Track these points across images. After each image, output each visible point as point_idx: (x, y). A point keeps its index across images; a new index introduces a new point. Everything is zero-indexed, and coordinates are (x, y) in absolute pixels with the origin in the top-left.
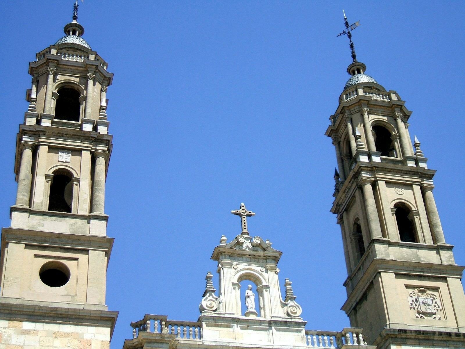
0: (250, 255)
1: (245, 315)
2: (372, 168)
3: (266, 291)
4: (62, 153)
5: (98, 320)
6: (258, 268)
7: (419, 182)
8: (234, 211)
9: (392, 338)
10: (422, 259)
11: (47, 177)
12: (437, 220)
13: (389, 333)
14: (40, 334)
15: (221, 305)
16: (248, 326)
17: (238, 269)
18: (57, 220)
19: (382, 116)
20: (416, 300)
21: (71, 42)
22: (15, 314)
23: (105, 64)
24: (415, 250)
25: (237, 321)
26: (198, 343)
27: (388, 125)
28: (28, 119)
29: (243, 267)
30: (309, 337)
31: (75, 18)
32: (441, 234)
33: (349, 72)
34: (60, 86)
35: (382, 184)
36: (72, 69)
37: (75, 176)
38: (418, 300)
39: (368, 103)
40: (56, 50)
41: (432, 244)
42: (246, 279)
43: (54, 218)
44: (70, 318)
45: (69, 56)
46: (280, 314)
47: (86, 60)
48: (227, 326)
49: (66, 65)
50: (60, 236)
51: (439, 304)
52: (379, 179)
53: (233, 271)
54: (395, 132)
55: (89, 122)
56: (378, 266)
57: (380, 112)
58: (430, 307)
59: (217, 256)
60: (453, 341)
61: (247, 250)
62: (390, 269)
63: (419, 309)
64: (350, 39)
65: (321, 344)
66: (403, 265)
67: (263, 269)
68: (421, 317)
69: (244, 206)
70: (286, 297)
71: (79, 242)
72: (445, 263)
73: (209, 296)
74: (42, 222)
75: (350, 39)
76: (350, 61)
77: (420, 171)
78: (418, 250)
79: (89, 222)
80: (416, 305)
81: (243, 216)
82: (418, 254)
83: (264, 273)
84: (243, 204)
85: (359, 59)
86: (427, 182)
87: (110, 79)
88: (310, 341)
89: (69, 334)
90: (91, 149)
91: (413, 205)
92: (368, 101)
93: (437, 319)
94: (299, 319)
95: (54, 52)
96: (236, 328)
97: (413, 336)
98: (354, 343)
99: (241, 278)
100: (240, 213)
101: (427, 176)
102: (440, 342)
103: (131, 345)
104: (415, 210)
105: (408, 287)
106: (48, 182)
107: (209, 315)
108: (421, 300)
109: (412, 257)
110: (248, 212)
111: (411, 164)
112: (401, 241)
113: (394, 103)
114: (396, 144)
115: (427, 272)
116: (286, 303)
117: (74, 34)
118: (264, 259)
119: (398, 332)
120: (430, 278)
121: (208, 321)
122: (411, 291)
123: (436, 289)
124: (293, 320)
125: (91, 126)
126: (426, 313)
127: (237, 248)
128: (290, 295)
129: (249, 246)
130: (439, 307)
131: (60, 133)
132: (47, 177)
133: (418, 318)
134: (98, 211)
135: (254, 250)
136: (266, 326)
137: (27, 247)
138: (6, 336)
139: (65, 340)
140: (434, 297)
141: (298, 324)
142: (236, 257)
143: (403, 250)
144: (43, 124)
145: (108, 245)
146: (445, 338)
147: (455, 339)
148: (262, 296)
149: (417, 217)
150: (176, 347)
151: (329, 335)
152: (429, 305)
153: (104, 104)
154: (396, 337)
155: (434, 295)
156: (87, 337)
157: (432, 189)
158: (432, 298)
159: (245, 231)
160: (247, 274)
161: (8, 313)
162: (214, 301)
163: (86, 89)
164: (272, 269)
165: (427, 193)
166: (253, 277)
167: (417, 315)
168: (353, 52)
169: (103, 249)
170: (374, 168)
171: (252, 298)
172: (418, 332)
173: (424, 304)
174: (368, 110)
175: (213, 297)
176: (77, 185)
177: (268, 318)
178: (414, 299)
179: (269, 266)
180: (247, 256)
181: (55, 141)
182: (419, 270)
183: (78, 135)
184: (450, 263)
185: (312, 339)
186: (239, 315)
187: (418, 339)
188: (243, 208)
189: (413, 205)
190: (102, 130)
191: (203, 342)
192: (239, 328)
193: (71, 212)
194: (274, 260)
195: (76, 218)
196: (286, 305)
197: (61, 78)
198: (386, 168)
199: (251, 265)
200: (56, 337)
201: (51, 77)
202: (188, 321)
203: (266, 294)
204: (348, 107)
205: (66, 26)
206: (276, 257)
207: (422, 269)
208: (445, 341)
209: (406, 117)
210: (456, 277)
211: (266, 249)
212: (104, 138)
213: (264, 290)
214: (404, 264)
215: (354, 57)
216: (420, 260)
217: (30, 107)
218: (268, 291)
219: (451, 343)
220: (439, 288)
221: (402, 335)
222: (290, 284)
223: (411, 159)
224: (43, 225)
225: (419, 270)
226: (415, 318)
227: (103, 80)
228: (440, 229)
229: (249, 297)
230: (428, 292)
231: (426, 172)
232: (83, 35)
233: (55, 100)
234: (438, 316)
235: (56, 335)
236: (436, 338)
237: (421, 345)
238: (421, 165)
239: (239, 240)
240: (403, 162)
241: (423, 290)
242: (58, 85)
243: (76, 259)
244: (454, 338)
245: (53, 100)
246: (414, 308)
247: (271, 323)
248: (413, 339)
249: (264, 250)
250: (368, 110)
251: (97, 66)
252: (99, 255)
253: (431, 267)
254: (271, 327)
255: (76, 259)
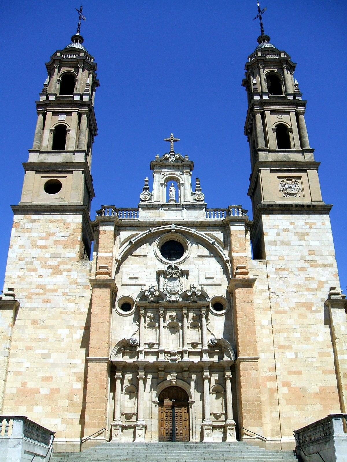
0: (173, 165)
1: (168, 202)
2: (261, 103)
3: (183, 186)
4: (61, 115)
5: (75, 211)
6: (178, 173)
7: (295, 109)
8: (166, 139)
9: (263, 210)
10: (291, 159)
11: (51, 130)
12: (305, 133)
13: (261, 207)
14: (41, 221)
15: (152, 197)
16: (169, 208)
17: (165, 174)
18: (55, 155)
19: (274, 68)
20: (284, 186)
21: (71, 47)
22: (27, 211)
23: (290, 58)
24: (287, 154)
25: (162, 206)
26: (136, 220)
27: (278, 74)
28: (41, 97)
29: (168, 173)
30: (208, 213)
31: (78, 32)
32: (307, 142)
33: (259, 41)
34: (63, 75)
35: (268, 113)
36: (70, 64)
37: (68, 128)
38: (285, 185)
39: (264, 61)
40: (60, 53)
41: (300, 149)
42: (171, 180)
43: (54, 154)
44: (59, 211)
45: (71, 55)
46: (190, 199)
47: (77, 57)
48: (155, 209)
49: (66, 62)
50: (55, 164)
51: (300, 187)
52: (266, 110)
53: (162, 176)
54: (282, 78)
55: (77, 94)
56: (259, 166)
57: (273, 66)
58: (293, 190)
59: (153, 167)
60: (306, 210)
61: (172, 162)
62: (267, 167)
63: (286, 192)
64: (261, 20)
65: (216, 217)
66: (276, 164)
67: (182, 173)
68: (287, 196)
69: (173, 136)
70: (195, 189)
71: (67, 167)
72: (307, 160)
73: (145, 192)
74: (47, 157)
75: (261, 20)
76: (260, 34)
77: (295, 102)
78: (289, 154)
79: (74, 155)
80: (284, 189)
81: (171, 142)
82: (288, 156)
83: (182, 176)
84: (172, 134)
85: (265, 33)
86: (301, 109)
87: (94, 66)
88: (209, 215)
89: (58, 220)
90: (78, 111)
91: (289, 125)
92: (264, 60)
93: (298, 197)
94: (202, 202)
95: (59, 54)
96: (161, 211)
97: (278, 208)
98: (239, 214)
99: (167, 180)
100: (169, 140)
101: (301, 105)
102: (296, 211)
103: (94, 224)
104: (290, 128)
105: (279, 177)
106: (51, 133)
107: (144, 203)
108: (287, 186)
109: (285, 158)
110: (175, 139)
111: (290, 98)
112: (278, 149)
113: (282, 59)
114: (282, 86)
115: (293, 168)
116: (195, 193)
117: (76, 42)
118: (183, 167)
119: (267, 206)
120: (295, 171)
121: (143, 207)
122: (281, 180)
123: (299, 178)
124: (198, 203)
125: (79, 97)
126: (291, 193)
127: (165, 162)
128: (198, 188)
129: (173, 160)
130: (300, 189)
131: (59, 103)
132: (51, 130)
133: (285, 197)
134: (80, 147)
135: (176, 162)
136: (180, 208)
137: (37, 172)
138: (22, 224)
139: (55, 224)
140: (298, 183)
141: (201, 205)
142: (164, 167)
143: (278, 154)
144: (50, 99)
145: (84, 167)
146: (300, 209)
147: (307, 209)
148: (180, 189)
149: (291, 133)
150: (121, 223)
151: (221, 211)
152: (293, 188)
153: (297, 83)
154: (266, 210)
155: (297, 182)
156: (68, 221)
157: (303, 113)
158: (295, 184)
159: (172, 151)
160: (171, 177)
161: (24, 211)
162: (148, 195)
163: (283, 75)
164: (187, 173)
165: (256, 115)
166: (175, 178)
167: (284, 195)
168: (262, 29)
169: (81, 170)
170: (263, 103)
171: (174, 191)
172: (281, 206)
173: (289, 187)
174: (263, 65)
175: (147, 193)
176: (69, 133)
177: (183, 203)
178: (283, 185)
179: (185, 171)
180: (172, 166)
181: (56, 109)
182: (287, 166)
183: (70, 103)
184: (311, 161)
185: (210, 214)
186: (164, 203)
187: (282, 210)
188: (171, 137)
189: (289, 125)
190: (299, 98)
191: (139, 220)
192: (162, 210)
193: (65, 150)
194: (189, 167)
195: (66, 153)
196: (195, 194)
197: (63, 70)
198: (271, 102)
199: (174, 171)
200: (50, 223)
201: (56, 70)
202: (131, 208)
203: (182, 188)
204: (251, 65)
205: (72, 38)
206: (190, 165)
207: (290, 166)
208: (300, 210)
209: (292, 68)
210: (314, 169)
211: (183, 160)
212: (86, 103)
213: (181, 186)
214: (276, 163)
215: (262, 32)
216: (290, 160)
217: (43, 90)
218: (184, 186)
219: (304, 211)
220: (301, 177)
221: (270, 208)
222: (199, 181)
223: (290, 95)
224: (47, 159)
225: (287, 166)
226: (282, 197)
227: (90, 67)
228: (307, 139)
229: (171, 191)
230: (293, 180)
231: (300, 102)
232: (83, 43)
233: (59, 84)
234: (298, 195)
235: (51, 221)
236: (294, 209)
237: (283, 214)
238: (297, 98)
239: (166, 156)
240: (285, 98)
241: (289, 179)
242: (61, 74)
243: (65, 177)
244: (306, 208)
245: (58, 84)
246: (282, 191)
247: (183, 206)
248: (277, 210)
249: (183, 161)
250: (263, 65)
251: (84, 60)
252: (79, 173)
253: (296, 164)
254: (183, 208)
255: (65, 177)
